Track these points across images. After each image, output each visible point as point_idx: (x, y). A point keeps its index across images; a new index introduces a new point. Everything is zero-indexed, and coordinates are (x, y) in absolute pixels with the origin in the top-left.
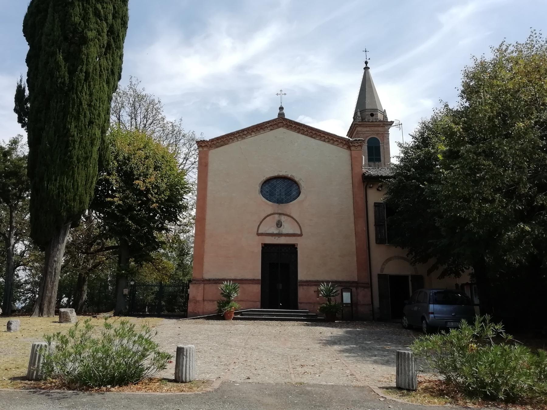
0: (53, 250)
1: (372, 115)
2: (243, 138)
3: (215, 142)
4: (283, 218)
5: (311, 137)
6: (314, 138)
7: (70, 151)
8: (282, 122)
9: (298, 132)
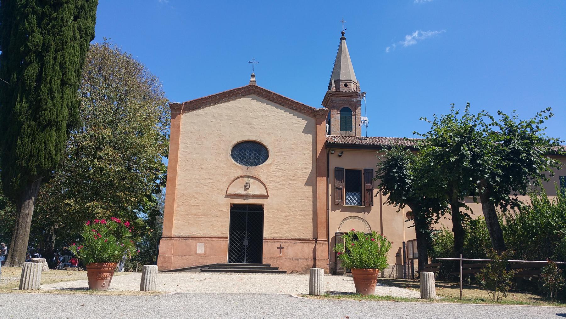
1: (346, 85)
3: (188, 106)
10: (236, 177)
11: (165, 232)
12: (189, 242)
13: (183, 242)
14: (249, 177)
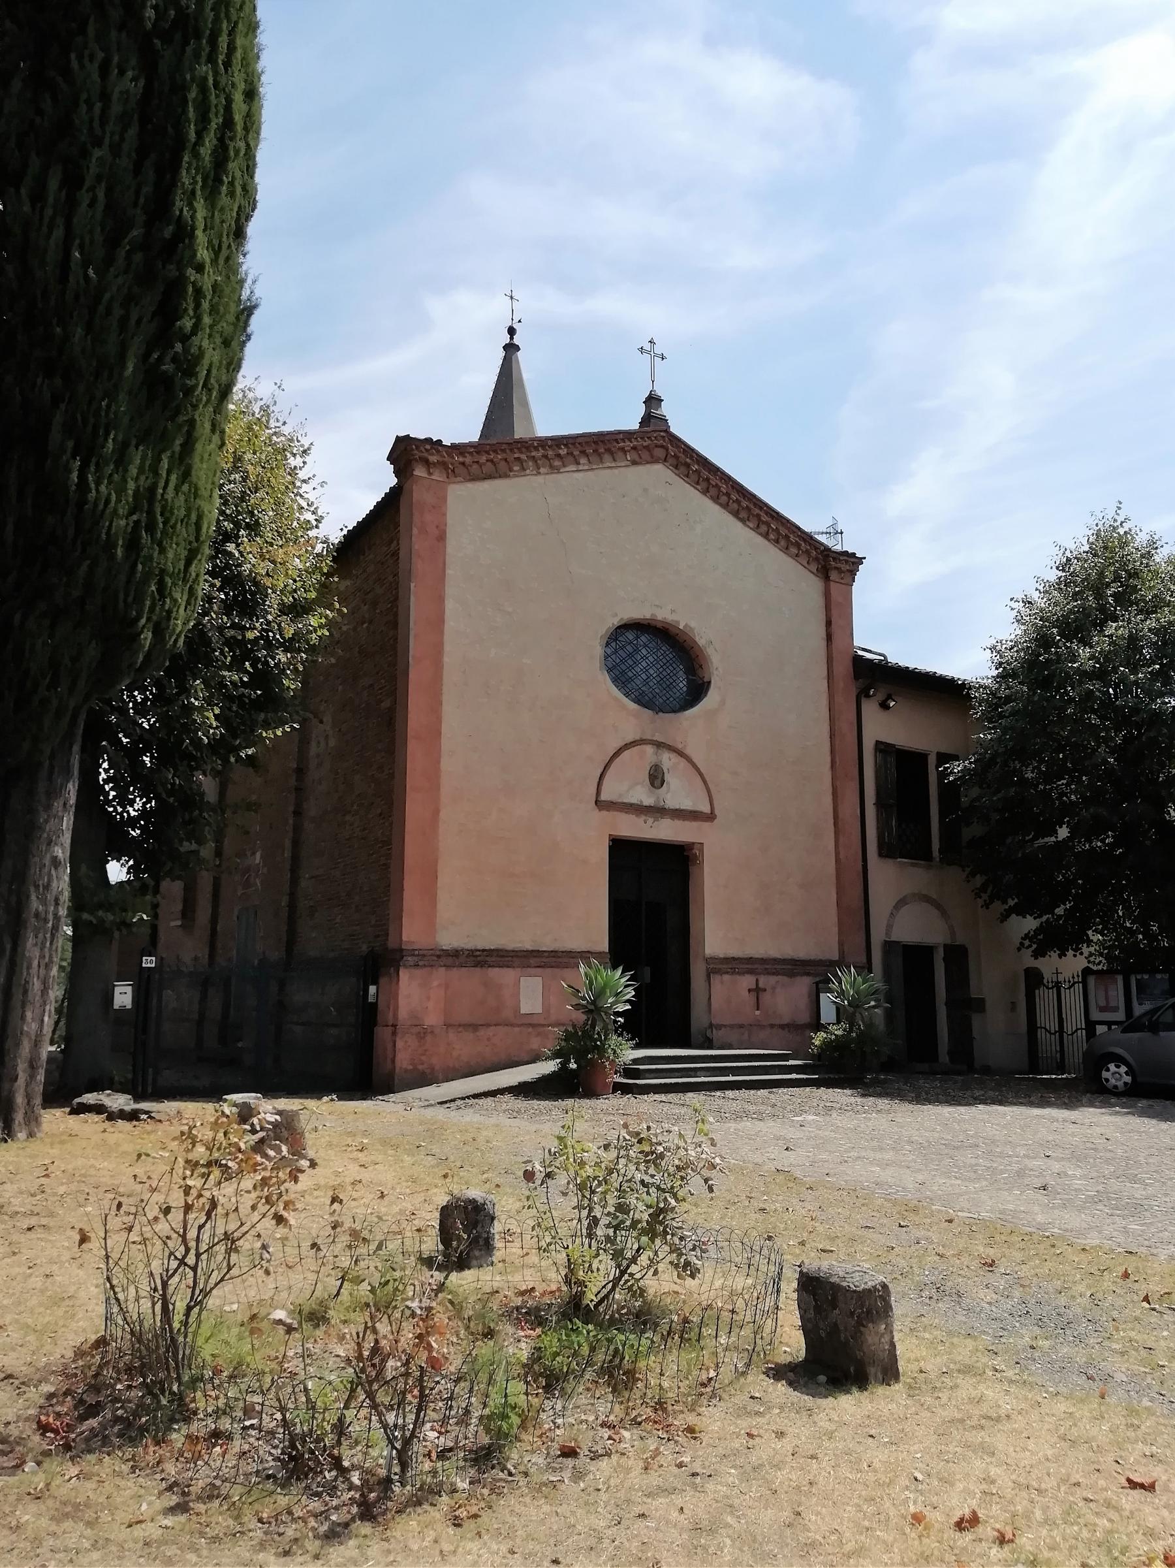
0: (48, 807)
2: (554, 469)
4: (667, 760)
5: (736, 514)
6: (742, 520)
7: (185, 339)
8: (653, 440)
9: (705, 492)
10: (621, 744)
11: (411, 933)
12: (496, 974)
13: (468, 981)
14: (659, 745)
